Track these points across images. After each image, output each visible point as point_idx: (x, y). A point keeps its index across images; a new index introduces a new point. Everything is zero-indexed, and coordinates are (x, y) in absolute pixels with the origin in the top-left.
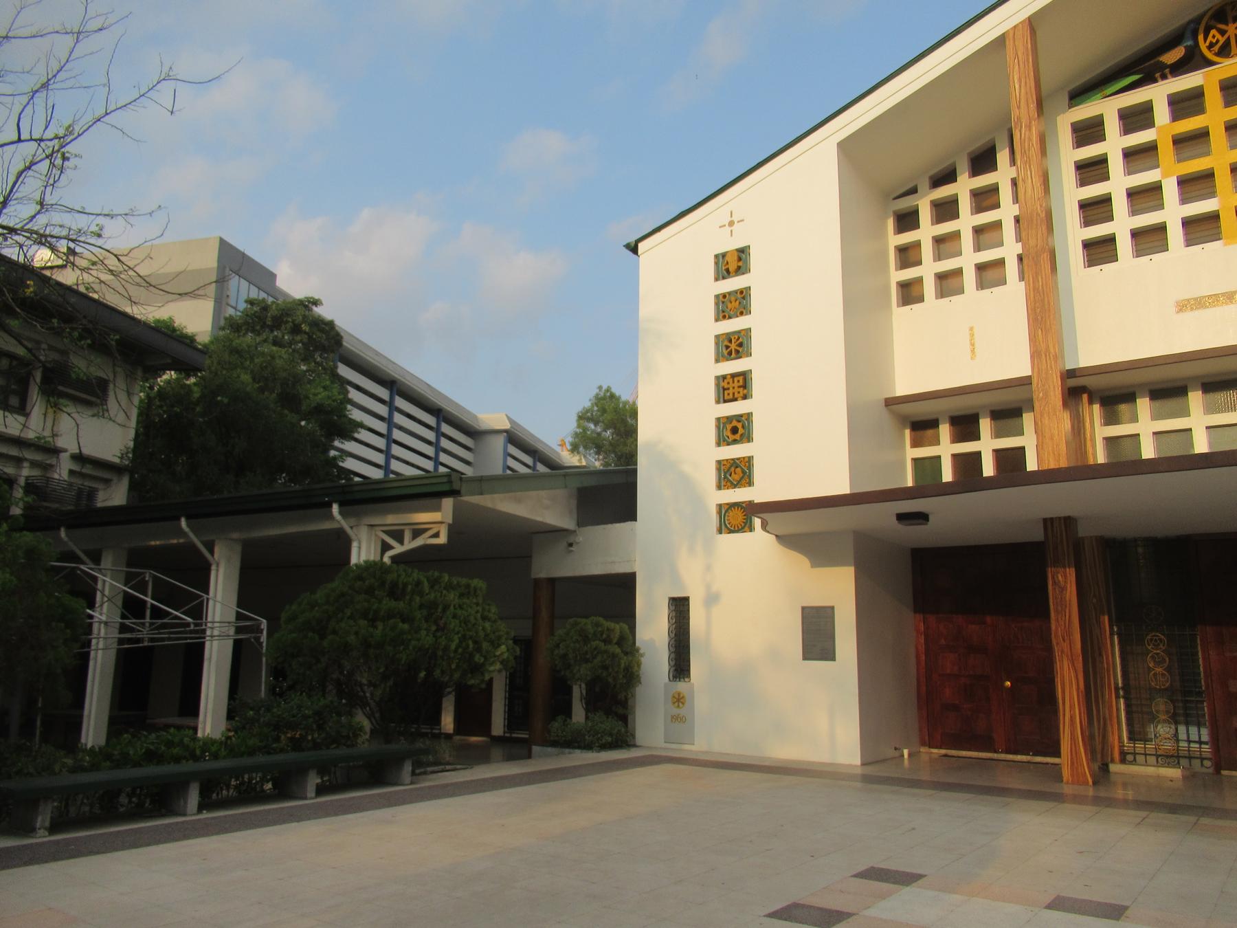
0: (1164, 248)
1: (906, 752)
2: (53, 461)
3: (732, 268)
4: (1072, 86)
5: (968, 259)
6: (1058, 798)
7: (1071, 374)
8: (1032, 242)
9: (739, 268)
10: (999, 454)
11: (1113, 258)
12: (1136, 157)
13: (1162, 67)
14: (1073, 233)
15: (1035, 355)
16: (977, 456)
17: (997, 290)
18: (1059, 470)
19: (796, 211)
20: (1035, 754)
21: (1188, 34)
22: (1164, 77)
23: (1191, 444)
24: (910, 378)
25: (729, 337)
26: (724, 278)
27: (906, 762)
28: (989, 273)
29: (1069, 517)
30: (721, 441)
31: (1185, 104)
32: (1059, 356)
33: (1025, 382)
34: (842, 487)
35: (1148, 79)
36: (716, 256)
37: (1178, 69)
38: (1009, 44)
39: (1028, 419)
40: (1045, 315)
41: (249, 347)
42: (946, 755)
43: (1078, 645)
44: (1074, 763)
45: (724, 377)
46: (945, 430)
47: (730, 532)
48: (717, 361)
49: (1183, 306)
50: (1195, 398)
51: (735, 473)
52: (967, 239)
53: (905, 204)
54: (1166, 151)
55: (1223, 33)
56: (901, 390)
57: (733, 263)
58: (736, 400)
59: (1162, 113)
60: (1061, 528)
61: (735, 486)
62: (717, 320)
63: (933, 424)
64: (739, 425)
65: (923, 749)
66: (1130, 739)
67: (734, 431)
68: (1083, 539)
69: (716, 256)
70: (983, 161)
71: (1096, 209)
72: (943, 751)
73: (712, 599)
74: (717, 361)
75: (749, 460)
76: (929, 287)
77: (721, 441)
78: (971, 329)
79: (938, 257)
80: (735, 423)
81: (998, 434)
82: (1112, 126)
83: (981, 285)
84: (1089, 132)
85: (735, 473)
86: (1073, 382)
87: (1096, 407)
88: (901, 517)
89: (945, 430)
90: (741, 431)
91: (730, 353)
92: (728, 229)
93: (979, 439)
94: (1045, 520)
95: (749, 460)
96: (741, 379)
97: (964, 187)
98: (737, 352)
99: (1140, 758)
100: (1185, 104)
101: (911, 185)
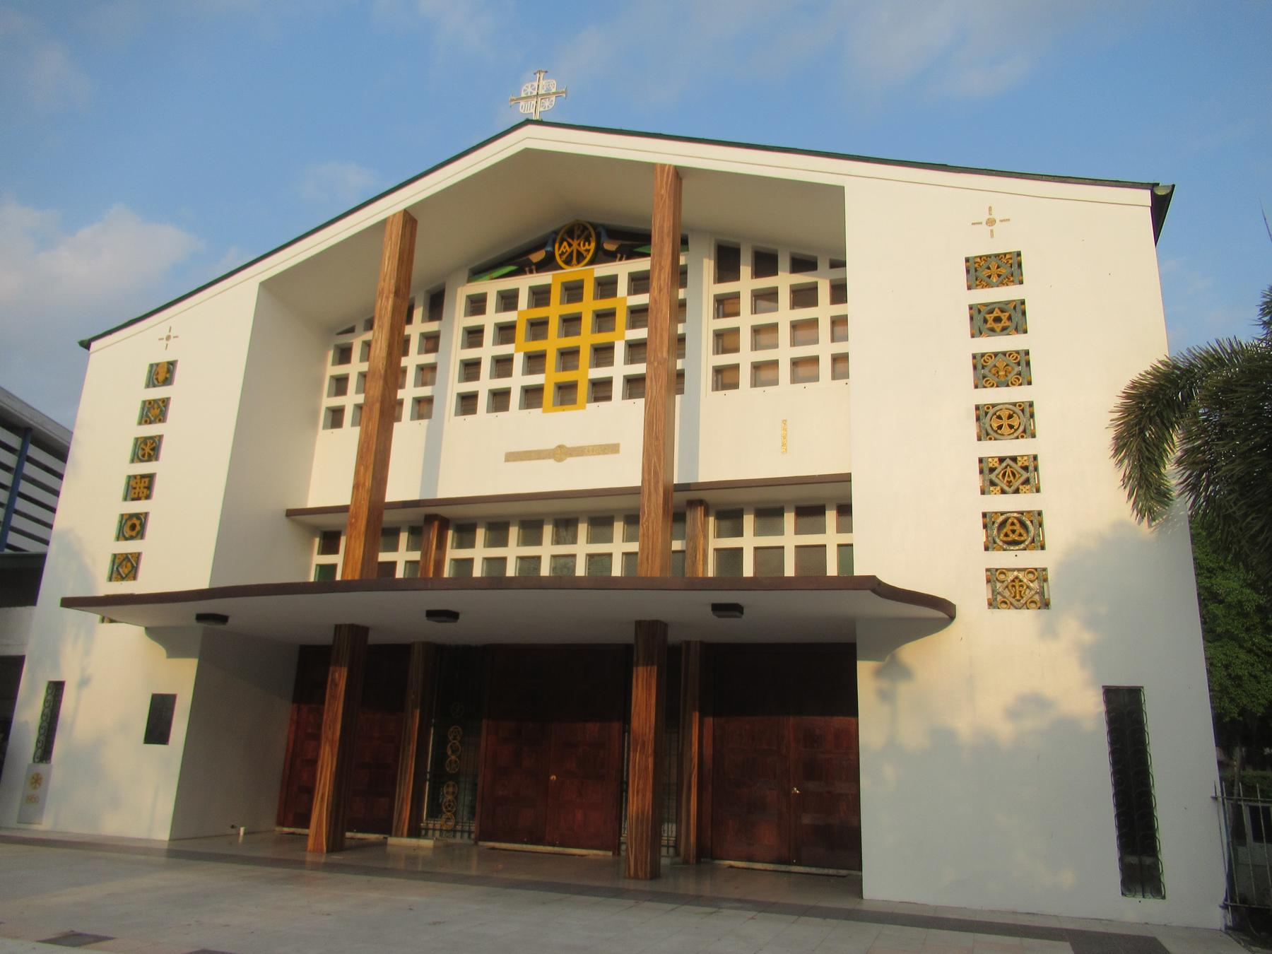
0: (608, 398)
1: (242, 830)
2: (574, 261)
3: (161, 378)
4: (477, 263)
5: (784, 352)
6: (301, 864)
8: (371, 392)
10: (591, 557)
12: (505, 332)
13: (530, 263)
14: (451, 386)
18: (652, 579)
19: (216, 335)
20: (358, 831)
21: (550, 242)
22: (531, 272)
23: (538, 569)
25: (145, 440)
27: (241, 839)
30: (121, 536)
38: (388, 227)
42: (293, 833)
43: (338, 733)
44: (318, 834)
45: (135, 477)
46: (789, 519)
48: (132, 461)
49: (512, 457)
51: (126, 566)
52: (784, 333)
55: (570, 245)
56: (314, 500)
57: (163, 374)
58: (139, 499)
60: (651, 630)
61: (123, 579)
62: (140, 423)
63: (819, 511)
64: (137, 523)
65: (278, 829)
67: (133, 527)
69: (151, 365)
70: (765, 264)
71: (471, 369)
72: (292, 830)
73: (84, 682)
75: (138, 556)
76: (745, 375)
77: (121, 536)
78: (784, 422)
79: (755, 346)
81: (592, 539)
83: (795, 379)
84: (477, 304)
85: (126, 566)
88: (201, 617)
90: (138, 528)
92: (164, 342)
95: (138, 556)
97: (784, 281)
98: (150, 455)
99: (430, 832)
100: (508, 301)
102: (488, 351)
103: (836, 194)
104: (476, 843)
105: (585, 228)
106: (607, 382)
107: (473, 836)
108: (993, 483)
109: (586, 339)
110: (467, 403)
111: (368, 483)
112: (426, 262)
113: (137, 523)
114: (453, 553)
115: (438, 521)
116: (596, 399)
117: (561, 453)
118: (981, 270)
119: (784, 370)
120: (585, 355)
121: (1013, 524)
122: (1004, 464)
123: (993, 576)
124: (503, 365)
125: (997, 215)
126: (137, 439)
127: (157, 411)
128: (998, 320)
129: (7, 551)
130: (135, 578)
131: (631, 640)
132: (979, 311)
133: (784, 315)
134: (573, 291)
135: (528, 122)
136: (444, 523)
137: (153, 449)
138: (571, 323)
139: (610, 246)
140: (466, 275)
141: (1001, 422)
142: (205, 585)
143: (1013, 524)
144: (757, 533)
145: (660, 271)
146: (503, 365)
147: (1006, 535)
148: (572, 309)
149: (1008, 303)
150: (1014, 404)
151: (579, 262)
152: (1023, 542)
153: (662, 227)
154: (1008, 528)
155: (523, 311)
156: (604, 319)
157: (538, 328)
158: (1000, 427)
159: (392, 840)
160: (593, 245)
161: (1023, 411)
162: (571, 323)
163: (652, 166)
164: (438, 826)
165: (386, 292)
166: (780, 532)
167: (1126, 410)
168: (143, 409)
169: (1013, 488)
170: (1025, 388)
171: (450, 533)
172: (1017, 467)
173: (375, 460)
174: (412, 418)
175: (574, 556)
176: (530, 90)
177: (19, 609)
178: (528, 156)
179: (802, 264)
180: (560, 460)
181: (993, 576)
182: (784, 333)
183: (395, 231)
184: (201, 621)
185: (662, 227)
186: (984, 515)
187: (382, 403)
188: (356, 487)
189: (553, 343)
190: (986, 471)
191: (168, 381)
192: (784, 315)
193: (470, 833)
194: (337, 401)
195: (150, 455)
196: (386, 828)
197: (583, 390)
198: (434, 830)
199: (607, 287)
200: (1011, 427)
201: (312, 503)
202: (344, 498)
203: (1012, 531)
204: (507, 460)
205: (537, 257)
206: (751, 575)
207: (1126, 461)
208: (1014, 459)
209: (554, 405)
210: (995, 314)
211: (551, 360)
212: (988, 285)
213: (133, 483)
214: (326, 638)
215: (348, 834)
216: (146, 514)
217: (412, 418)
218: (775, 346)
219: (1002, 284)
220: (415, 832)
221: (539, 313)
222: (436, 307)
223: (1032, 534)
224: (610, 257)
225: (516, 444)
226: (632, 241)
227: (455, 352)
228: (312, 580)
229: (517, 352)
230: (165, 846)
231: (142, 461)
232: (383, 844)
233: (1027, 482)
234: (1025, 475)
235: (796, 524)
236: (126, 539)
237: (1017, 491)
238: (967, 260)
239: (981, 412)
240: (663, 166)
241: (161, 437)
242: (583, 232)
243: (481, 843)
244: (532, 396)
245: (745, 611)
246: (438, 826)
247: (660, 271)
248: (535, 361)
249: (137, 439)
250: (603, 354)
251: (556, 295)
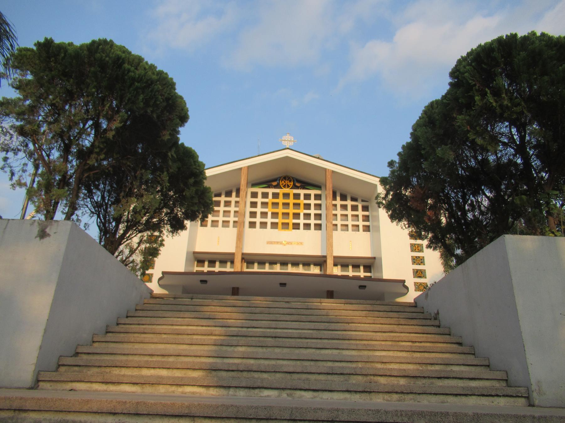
7: (243, 254)
12: (264, 204)
15: (237, 247)
24: (199, 248)
28: (226, 224)
31: (275, 195)
32: (242, 249)
33: (233, 254)
35: (269, 187)
37: (276, 187)
38: (243, 170)
40: (240, 238)
41: (440, 247)
46: (206, 263)
50: (312, 266)
54: (270, 205)
56: (197, 249)
63: (347, 266)
70: (228, 194)
71: (253, 214)
78: (301, 243)
82: (260, 195)
83: (223, 226)
84: (254, 195)
87: (245, 264)
89: (206, 263)
105: (289, 178)
119: (220, 223)
124: (264, 215)
133: (349, 212)
139: (298, 184)
160: (292, 183)
179: (353, 199)
199: (297, 196)
205: (275, 184)
224: (297, 188)
226: (305, 185)
244: (274, 225)
250: (297, 216)
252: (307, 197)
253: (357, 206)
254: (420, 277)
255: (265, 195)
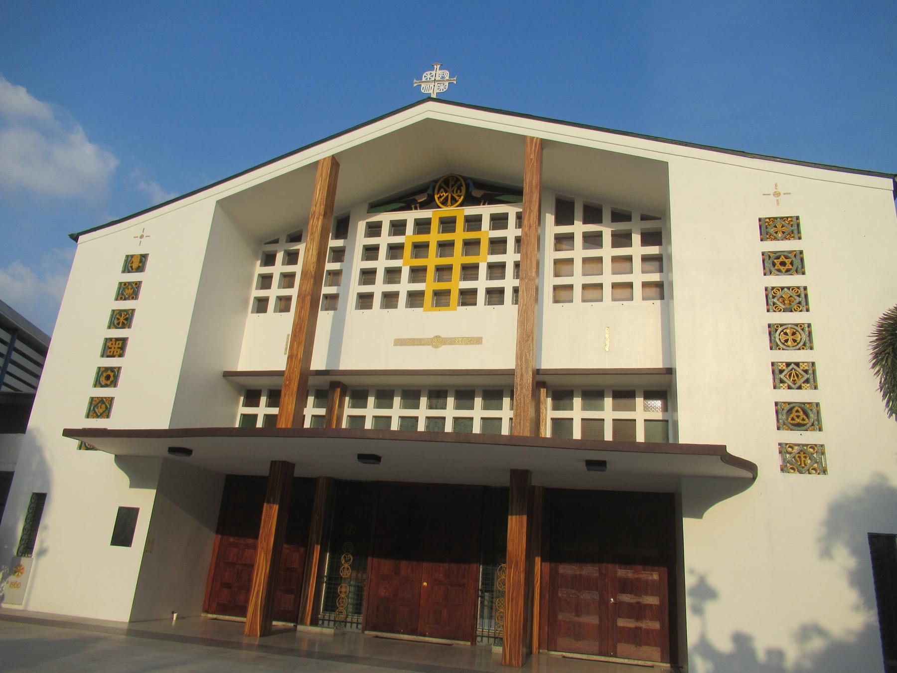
1: (175, 615)
3: (135, 266)
4: (375, 200)
7: (538, 372)
9: (139, 267)
11: (501, 302)
14: (354, 287)
16: (416, 419)
17: (566, 305)
21: (431, 188)
22: (416, 209)
26: (129, 272)
27: (174, 623)
28: (495, 296)
29: (288, 463)
30: (98, 383)
33: (510, 373)
34: (164, 424)
35: (407, 208)
36: (127, 256)
37: (424, 206)
38: (320, 168)
39: (506, 401)
42: (215, 619)
44: (253, 622)
45: (111, 339)
47: (87, 449)
48: (109, 327)
49: (399, 342)
50: (639, 401)
51: (100, 407)
53: (270, 248)
56: (243, 365)
58: (113, 356)
59: (410, 228)
60: (284, 468)
61: (98, 417)
62: (116, 299)
64: (112, 374)
66: (325, 609)
67: (108, 377)
68: (534, 487)
69: (127, 256)
71: (368, 276)
72: (215, 616)
74: (109, 327)
77: (98, 383)
80: (109, 372)
81: (378, 406)
84: (374, 229)
85: (100, 407)
86: (540, 378)
88: (172, 450)
90: (112, 378)
91: (118, 324)
92: (139, 240)
93: (572, 409)
94: (272, 462)
96: (121, 342)
97: (578, 228)
98: (123, 323)
99: (326, 623)
101: (276, 238)
102: (382, 263)
103: (661, 168)
104: (363, 632)
105: (458, 180)
106: (474, 292)
107: (360, 626)
108: (782, 381)
109: (458, 259)
110: (365, 301)
111: (300, 355)
112: (344, 193)
113: (112, 374)
114: (349, 411)
115: (336, 387)
116: (464, 304)
117: (437, 342)
118: (770, 228)
120: (457, 271)
121: (797, 411)
122: (790, 368)
123: (784, 448)
124: (393, 274)
125: (781, 190)
126: (113, 311)
127: (131, 291)
128: (783, 264)
129: (5, 389)
130: (108, 417)
131: (508, 484)
132: (770, 257)
133: (607, 251)
134: (448, 224)
135: (430, 99)
136: (345, 389)
137: (126, 319)
138: (445, 247)
139: (477, 193)
140: (366, 207)
141: (787, 337)
142: (165, 426)
143: (797, 411)
144: (584, 408)
145: (530, 213)
146: (393, 274)
147: (793, 419)
148: (447, 237)
149: (790, 252)
150: (797, 325)
151: (452, 204)
152: (804, 425)
153: (531, 182)
154: (794, 414)
155: (409, 237)
156: (471, 245)
157: (420, 248)
158: (786, 341)
159: (300, 628)
161: (803, 330)
162: (445, 247)
163: (523, 138)
164: (332, 618)
165: (317, 215)
166: (444, 407)
167: (880, 333)
168: (119, 288)
169: (797, 385)
170: (804, 313)
171: (347, 399)
172: (799, 370)
173: (303, 337)
174: (275, 311)
175: (472, 419)
176: (429, 76)
177: (11, 435)
178: (428, 124)
179: (619, 216)
180: (436, 347)
181: (784, 448)
182: (578, 265)
183: (325, 170)
184: (161, 456)
185: (531, 182)
186: (776, 404)
187: (312, 295)
188: (290, 357)
189: (432, 260)
190: (777, 372)
191: (140, 269)
192: (607, 251)
193: (358, 623)
194: (263, 293)
195: (123, 323)
196: (295, 617)
197: (455, 296)
198: (329, 620)
199: (474, 222)
200: (795, 341)
201: (241, 368)
202: (280, 364)
203: (797, 416)
204: (395, 345)
205: (422, 199)
206: (643, 441)
207: (881, 372)
208: (797, 364)
209: (432, 306)
210: (781, 260)
211: (431, 273)
212: (775, 239)
213: (109, 344)
214: (264, 470)
215: (274, 623)
216: (119, 368)
217: (275, 311)
218: (571, 275)
219: (785, 238)
220: (314, 622)
221: (422, 238)
222: (342, 228)
223: (812, 420)
224: (475, 202)
225: (412, 334)
226: (507, 191)
227: (357, 263)
228: (237, 426)
229: (404, 264)
230: (126, 627)
231: (116, 328)
232: (294, 630)
233: (807, 381)
234: (806, 376)
235: (613, 404)
236: (102, 386)
237: (800, 388)
238: (760, 220)
239: (772, 329)
240: (532, 138)
241: (133, 310)
242: (456, 182)
243: (367, 632)
244: (415, 299)
245: (608, 465)
246: (332, 618)
247: (530, 213)
248: (418, 273)
249: (113, 311)
250: (470, 271)
251: (435, 226)
252: (499, 221)
253: (599, 235)
254: (799, 426)
255: (398, 228)
